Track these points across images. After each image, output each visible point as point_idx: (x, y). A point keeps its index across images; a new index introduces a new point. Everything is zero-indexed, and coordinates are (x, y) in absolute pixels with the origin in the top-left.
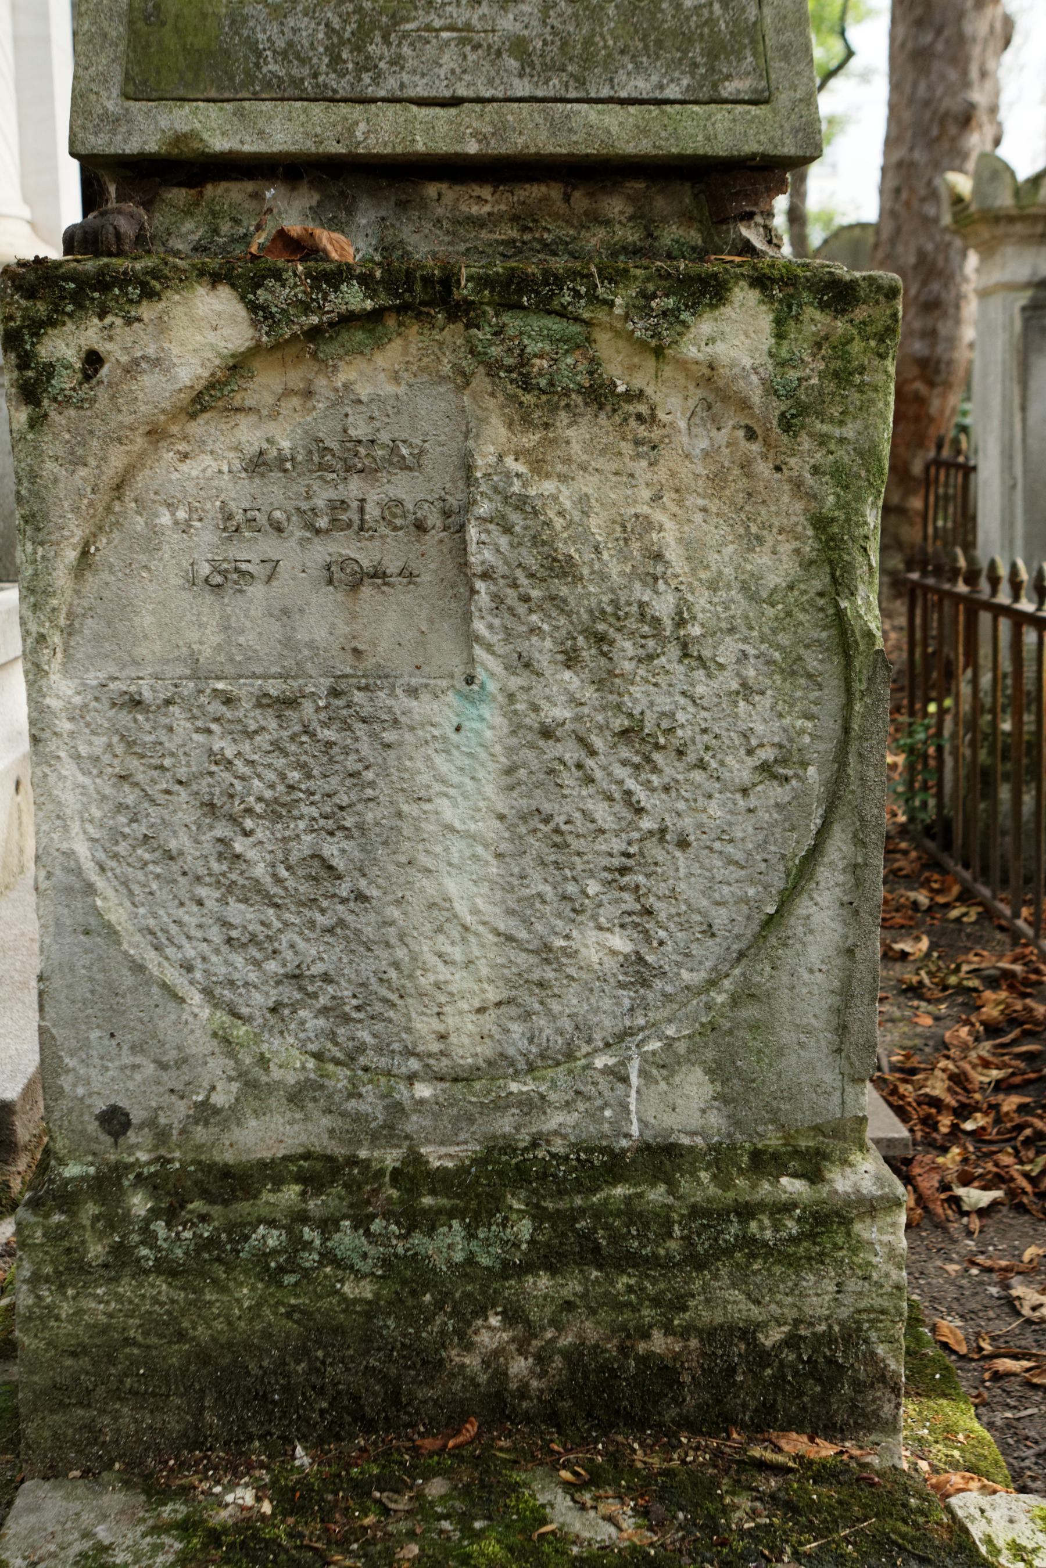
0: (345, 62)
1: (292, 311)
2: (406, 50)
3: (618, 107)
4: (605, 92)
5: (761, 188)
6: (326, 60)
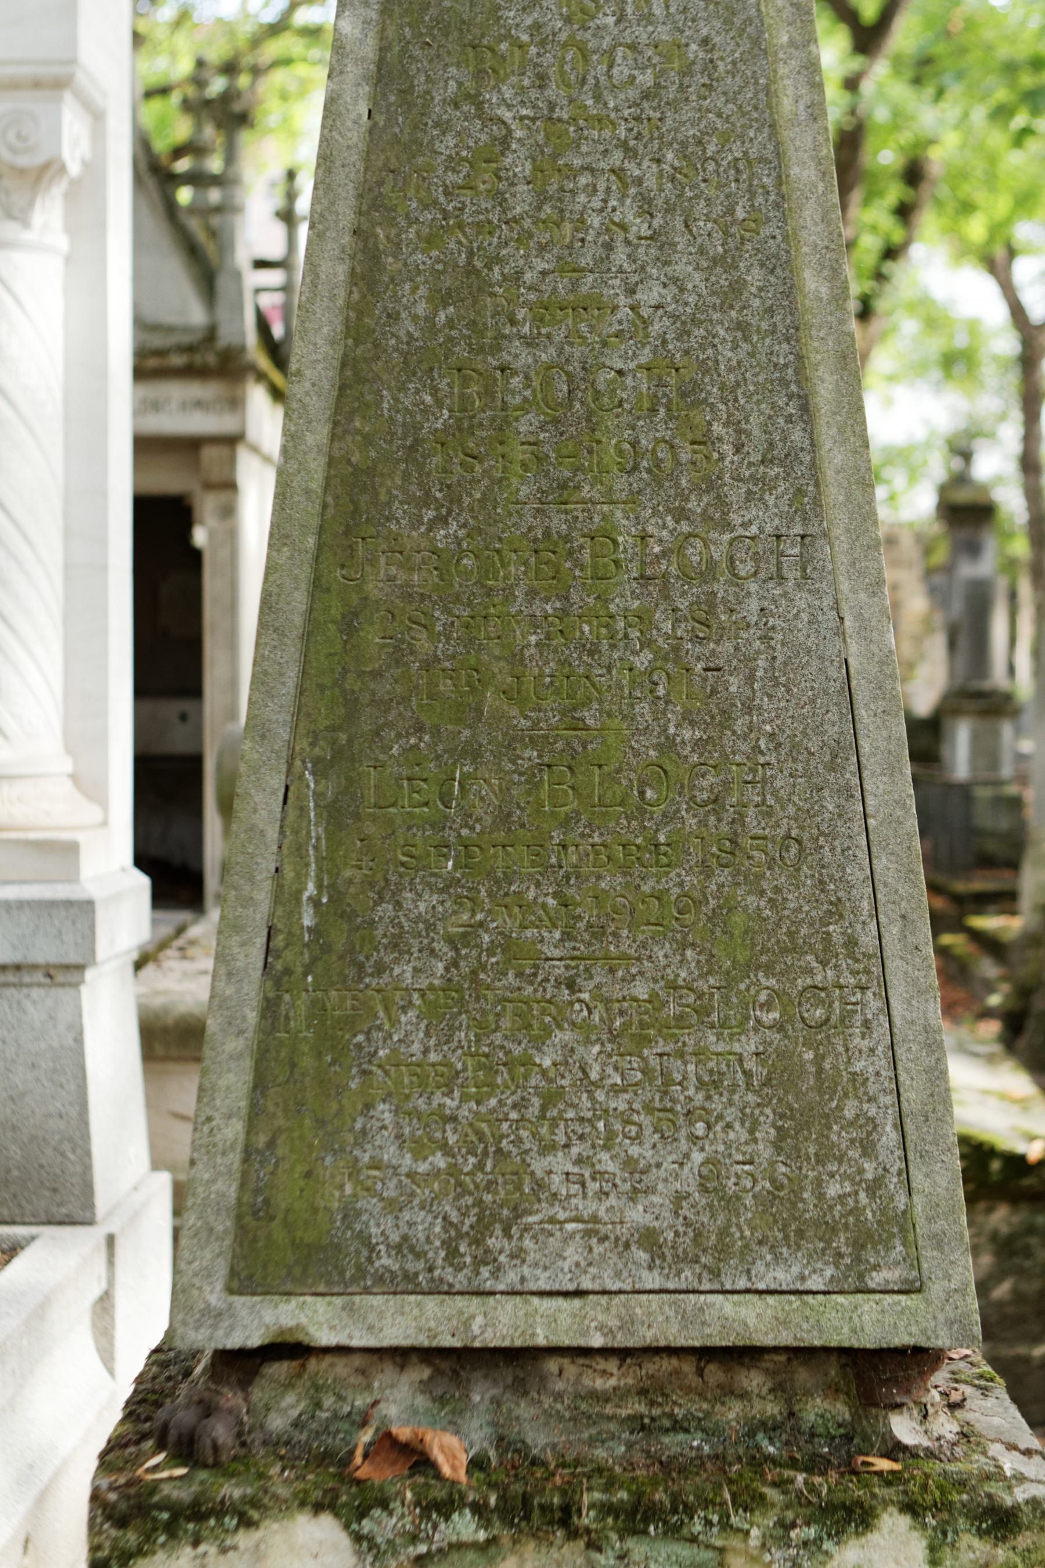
0: (463, 1256)
1: (398, 1541)
2: (528, 1243)
3: (755, 1298)
4: (742, 1283)
5: (914, 1373)
6: (442, 1254)
